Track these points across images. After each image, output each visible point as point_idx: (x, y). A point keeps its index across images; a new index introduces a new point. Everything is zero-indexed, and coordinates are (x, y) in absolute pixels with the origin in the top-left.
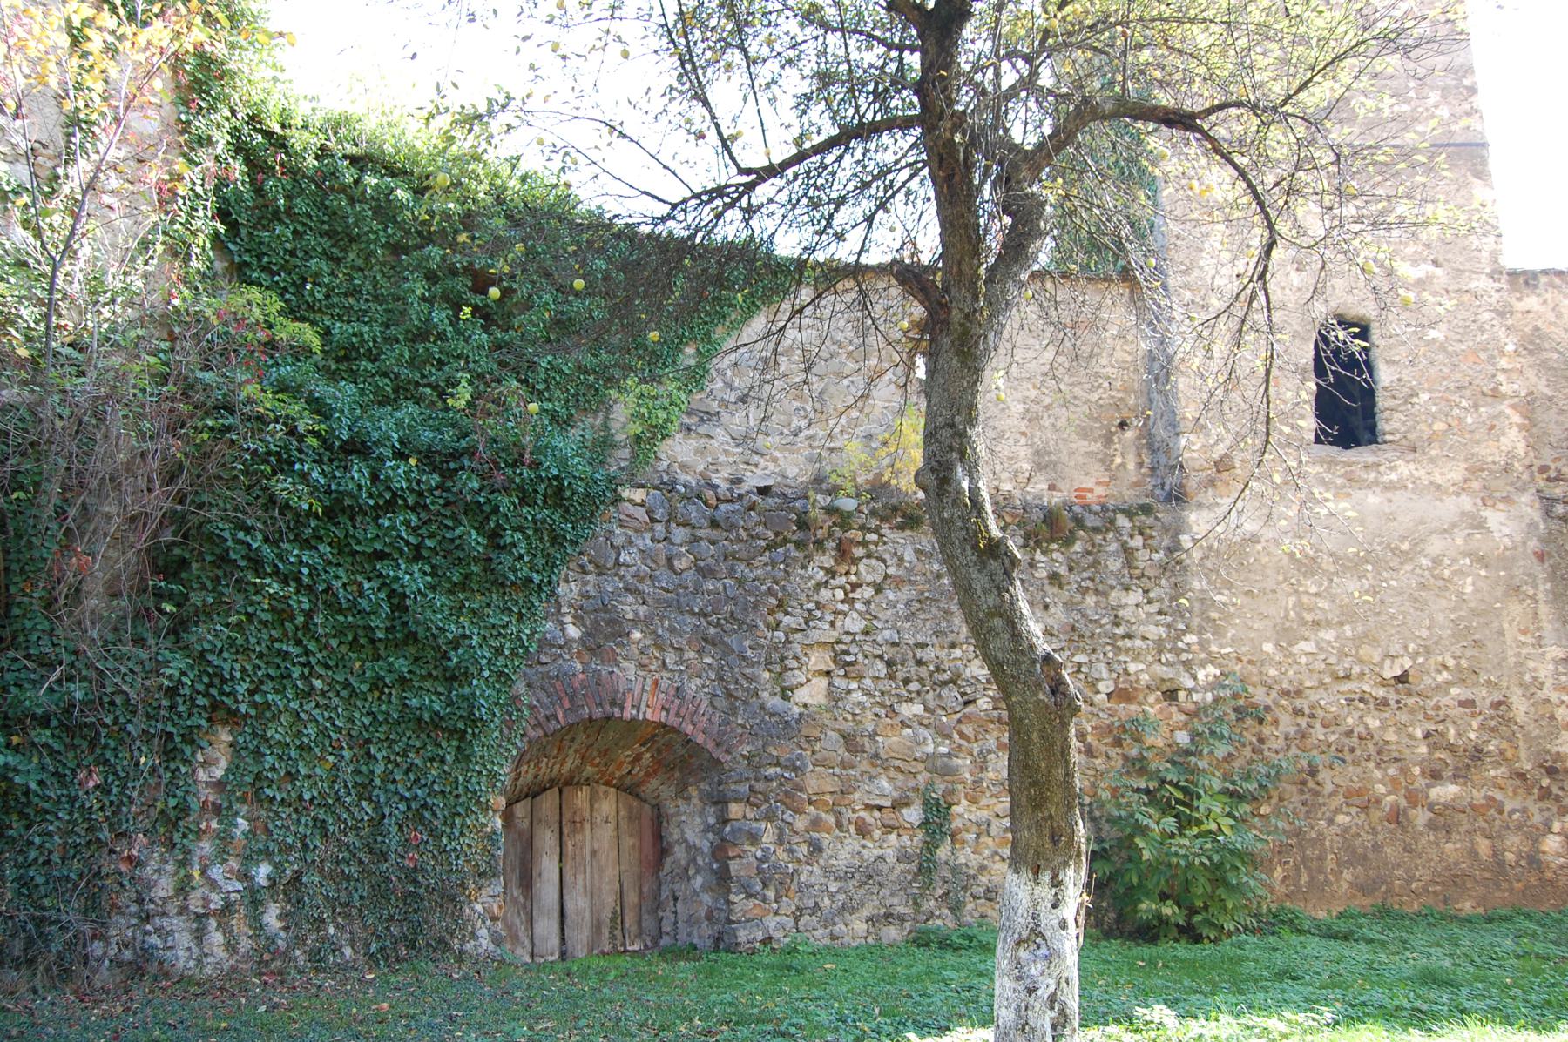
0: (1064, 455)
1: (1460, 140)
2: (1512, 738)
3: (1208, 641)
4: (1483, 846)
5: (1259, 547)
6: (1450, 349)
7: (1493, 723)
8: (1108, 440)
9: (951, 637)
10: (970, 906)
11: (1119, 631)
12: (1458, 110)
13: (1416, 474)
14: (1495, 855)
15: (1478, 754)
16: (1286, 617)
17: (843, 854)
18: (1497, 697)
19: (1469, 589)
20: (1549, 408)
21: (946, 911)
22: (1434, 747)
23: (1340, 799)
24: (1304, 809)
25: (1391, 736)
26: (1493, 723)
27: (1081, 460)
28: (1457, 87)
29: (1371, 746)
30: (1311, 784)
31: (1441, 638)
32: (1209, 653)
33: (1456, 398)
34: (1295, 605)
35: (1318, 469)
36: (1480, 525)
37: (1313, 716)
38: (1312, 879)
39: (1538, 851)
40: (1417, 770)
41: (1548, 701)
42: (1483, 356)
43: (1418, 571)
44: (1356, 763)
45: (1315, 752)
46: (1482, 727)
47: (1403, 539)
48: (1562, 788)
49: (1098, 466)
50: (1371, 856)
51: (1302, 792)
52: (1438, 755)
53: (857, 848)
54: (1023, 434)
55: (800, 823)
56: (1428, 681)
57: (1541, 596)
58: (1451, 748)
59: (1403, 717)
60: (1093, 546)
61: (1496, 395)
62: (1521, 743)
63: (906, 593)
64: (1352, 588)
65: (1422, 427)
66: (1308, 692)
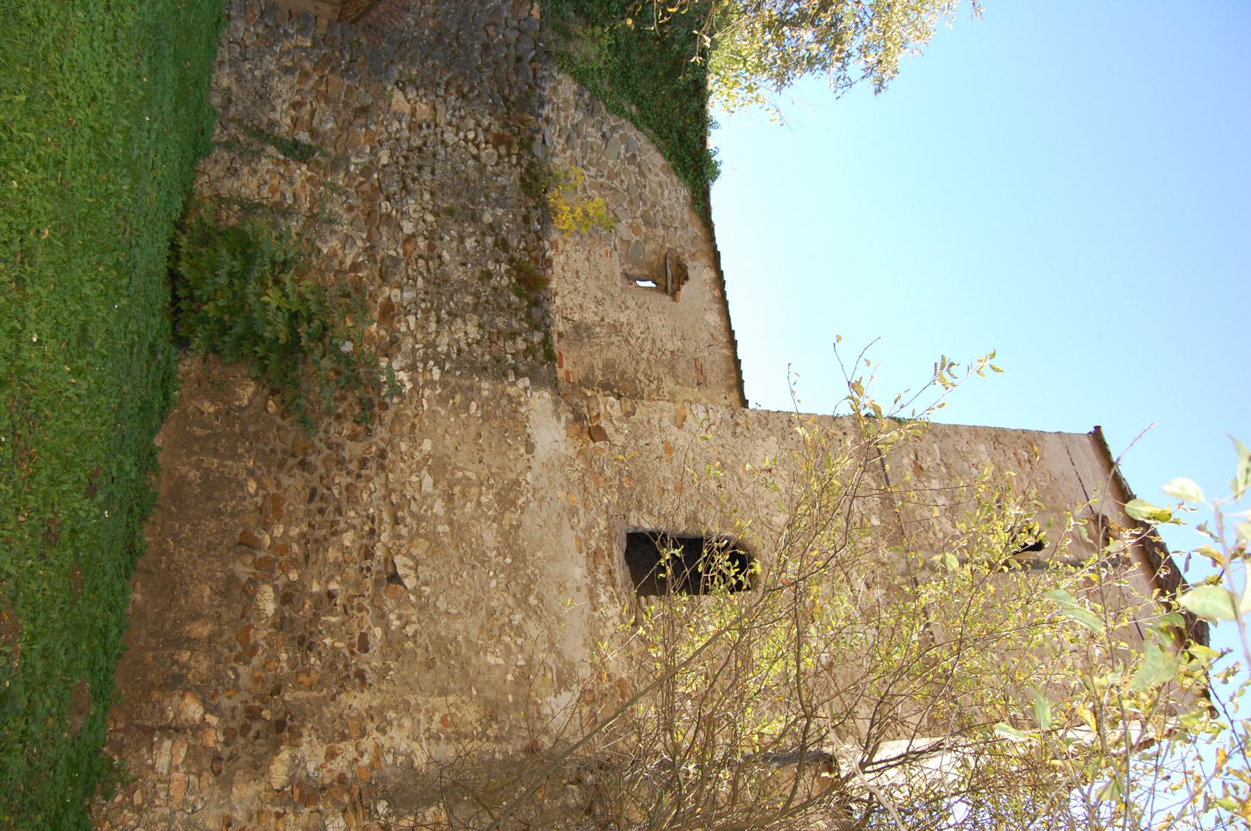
0: (587, 349)
3: (434, 389)
4: (202, 630)
5: (522, 450)
7: (341, 667)
9: (439, 194)
10: (226, 155)
13: (609, 624)
14: (188, 640)
15: (306, 644)
17: (281, 87)
18: (371, 677)
19: (491, 659)
21: (225, 139)
23: (272, 490)
24: (267, 449)
25: (332, 554)
27: (586, 360)
29: (324, 532)
30: (291, 462)
31: (436, 623)
32: (423, 388)
34: (468, 479)
35: (602, 523)
36: (562, 683)
37: (359, 476)
38: (197, 439)
39: (185, 690)
40: (294, 576)
41: (363, 733)
43: (507, 611)
44: (308, 513)
45: (322, 470)
47: (540, 598)
48: (257, 737)
50: (209, 506)
51: (284, 452)
53: (284, 97)
54: (603, 320)
55: (308, 66)
56: (390, 603)
59: (351, 571)
62: (314, 693)
63: (473, 174)
64: (490, 536)
66: (383, 476)
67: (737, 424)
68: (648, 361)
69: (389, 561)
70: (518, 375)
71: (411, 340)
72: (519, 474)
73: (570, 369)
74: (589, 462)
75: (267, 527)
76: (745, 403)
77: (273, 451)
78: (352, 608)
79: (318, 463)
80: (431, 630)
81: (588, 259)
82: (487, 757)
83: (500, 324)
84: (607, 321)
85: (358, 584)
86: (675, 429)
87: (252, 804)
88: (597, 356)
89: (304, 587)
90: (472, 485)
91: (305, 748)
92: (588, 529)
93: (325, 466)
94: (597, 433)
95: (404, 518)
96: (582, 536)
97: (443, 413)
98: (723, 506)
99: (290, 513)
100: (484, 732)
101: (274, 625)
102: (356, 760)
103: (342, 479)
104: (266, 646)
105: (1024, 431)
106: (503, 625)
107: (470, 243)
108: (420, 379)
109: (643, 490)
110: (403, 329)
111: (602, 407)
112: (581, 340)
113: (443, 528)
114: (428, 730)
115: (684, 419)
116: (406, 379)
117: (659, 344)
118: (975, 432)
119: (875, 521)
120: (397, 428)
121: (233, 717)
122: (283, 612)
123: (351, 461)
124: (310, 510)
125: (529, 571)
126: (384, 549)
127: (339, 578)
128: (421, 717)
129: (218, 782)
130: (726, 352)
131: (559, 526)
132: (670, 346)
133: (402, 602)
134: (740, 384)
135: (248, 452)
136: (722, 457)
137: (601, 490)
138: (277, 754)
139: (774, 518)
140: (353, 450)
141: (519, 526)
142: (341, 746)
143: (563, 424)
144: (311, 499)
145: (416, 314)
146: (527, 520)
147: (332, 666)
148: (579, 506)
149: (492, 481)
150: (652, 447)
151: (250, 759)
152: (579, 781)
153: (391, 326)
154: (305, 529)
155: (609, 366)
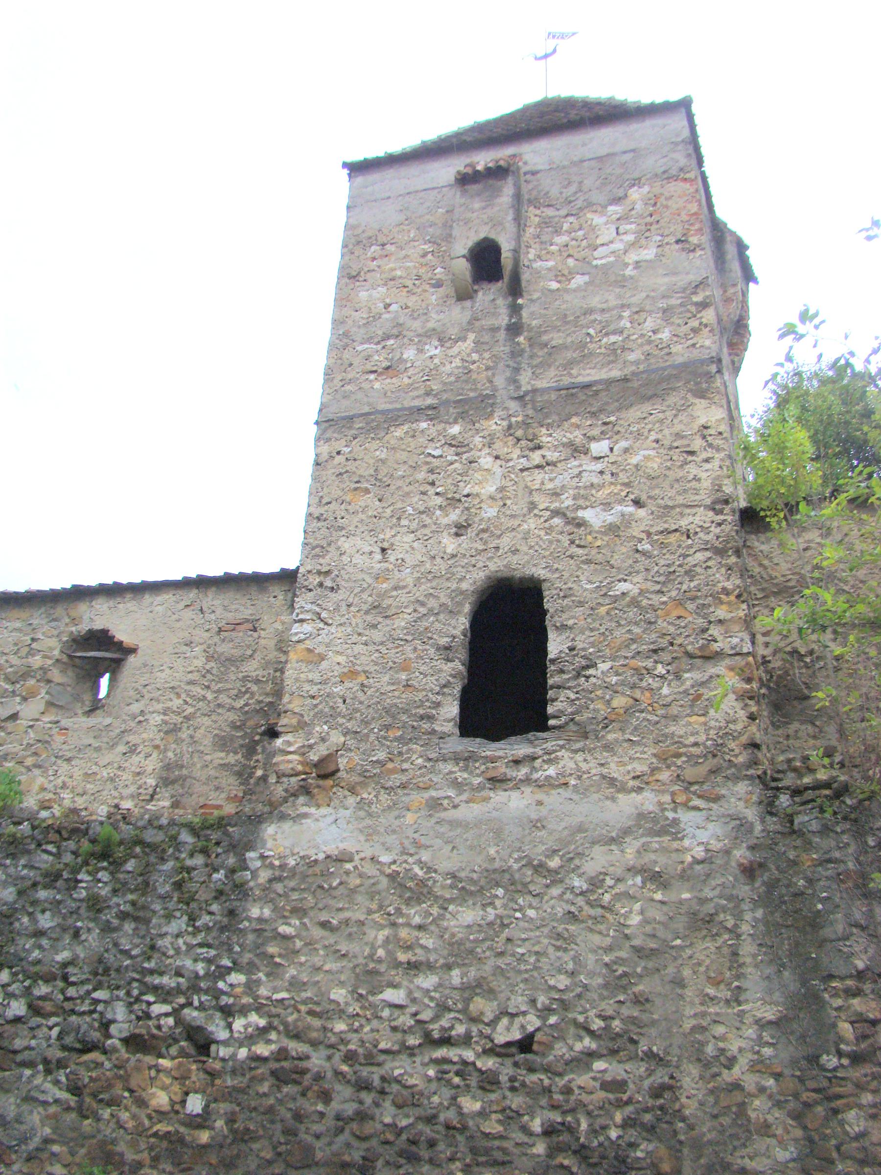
3: (258, 982)
5: (349, 866)
6: (645, 602)
7: (647, 1117)
13: (584, 766)
18: (661, 1076)
19: (635, 920)
26: (647, 1117)
32: (256, 998)
33: (649, 663)
34: (387, 941)
35: (449, 767)
36: (670, 829)
37: (382, 1092)
42: (691, 606)
49: (232, 780)
54: (157, 747)
56: (560, 1049)
57: (745, 928)
58: (582, 1152)
59: (516, 1101)
65: (599, 705)
67: (321, 585)
68: (219, 691)
71: (186, 1011)
73: (223, 796)
76: (288, 577)
80: (595, 996)
81: (69, 760)
82: (761, 927)
84: (158, 742)
86: (324, 665)
88: (208, 758)
90: (396, 935)
92: (456, 784)
94: (325, 771)
95: (443, 1029)
97: (292, 971)
100: (729, 931)
103: (387, 1114)
105: (345, 246)
107: (46, 921)
109: (405, 711)
112: (184, 778)
113: (456, 977)
114: (727, 1001)
117: (195, 676)
118: (343, 300)
119: (455, 429)
120: (314, 1035)
123: (361, 1102)
125: (516, 866)
127: (526, 1118)
131: (454, 824)
136: (365, 607)
141: (454, 876)
143: (313, 810)
145: (149, 1004)
146: (445, 865)
147: (651, 1130)
149: (391, 909)
150: (349, 695)
155: (222, 743)
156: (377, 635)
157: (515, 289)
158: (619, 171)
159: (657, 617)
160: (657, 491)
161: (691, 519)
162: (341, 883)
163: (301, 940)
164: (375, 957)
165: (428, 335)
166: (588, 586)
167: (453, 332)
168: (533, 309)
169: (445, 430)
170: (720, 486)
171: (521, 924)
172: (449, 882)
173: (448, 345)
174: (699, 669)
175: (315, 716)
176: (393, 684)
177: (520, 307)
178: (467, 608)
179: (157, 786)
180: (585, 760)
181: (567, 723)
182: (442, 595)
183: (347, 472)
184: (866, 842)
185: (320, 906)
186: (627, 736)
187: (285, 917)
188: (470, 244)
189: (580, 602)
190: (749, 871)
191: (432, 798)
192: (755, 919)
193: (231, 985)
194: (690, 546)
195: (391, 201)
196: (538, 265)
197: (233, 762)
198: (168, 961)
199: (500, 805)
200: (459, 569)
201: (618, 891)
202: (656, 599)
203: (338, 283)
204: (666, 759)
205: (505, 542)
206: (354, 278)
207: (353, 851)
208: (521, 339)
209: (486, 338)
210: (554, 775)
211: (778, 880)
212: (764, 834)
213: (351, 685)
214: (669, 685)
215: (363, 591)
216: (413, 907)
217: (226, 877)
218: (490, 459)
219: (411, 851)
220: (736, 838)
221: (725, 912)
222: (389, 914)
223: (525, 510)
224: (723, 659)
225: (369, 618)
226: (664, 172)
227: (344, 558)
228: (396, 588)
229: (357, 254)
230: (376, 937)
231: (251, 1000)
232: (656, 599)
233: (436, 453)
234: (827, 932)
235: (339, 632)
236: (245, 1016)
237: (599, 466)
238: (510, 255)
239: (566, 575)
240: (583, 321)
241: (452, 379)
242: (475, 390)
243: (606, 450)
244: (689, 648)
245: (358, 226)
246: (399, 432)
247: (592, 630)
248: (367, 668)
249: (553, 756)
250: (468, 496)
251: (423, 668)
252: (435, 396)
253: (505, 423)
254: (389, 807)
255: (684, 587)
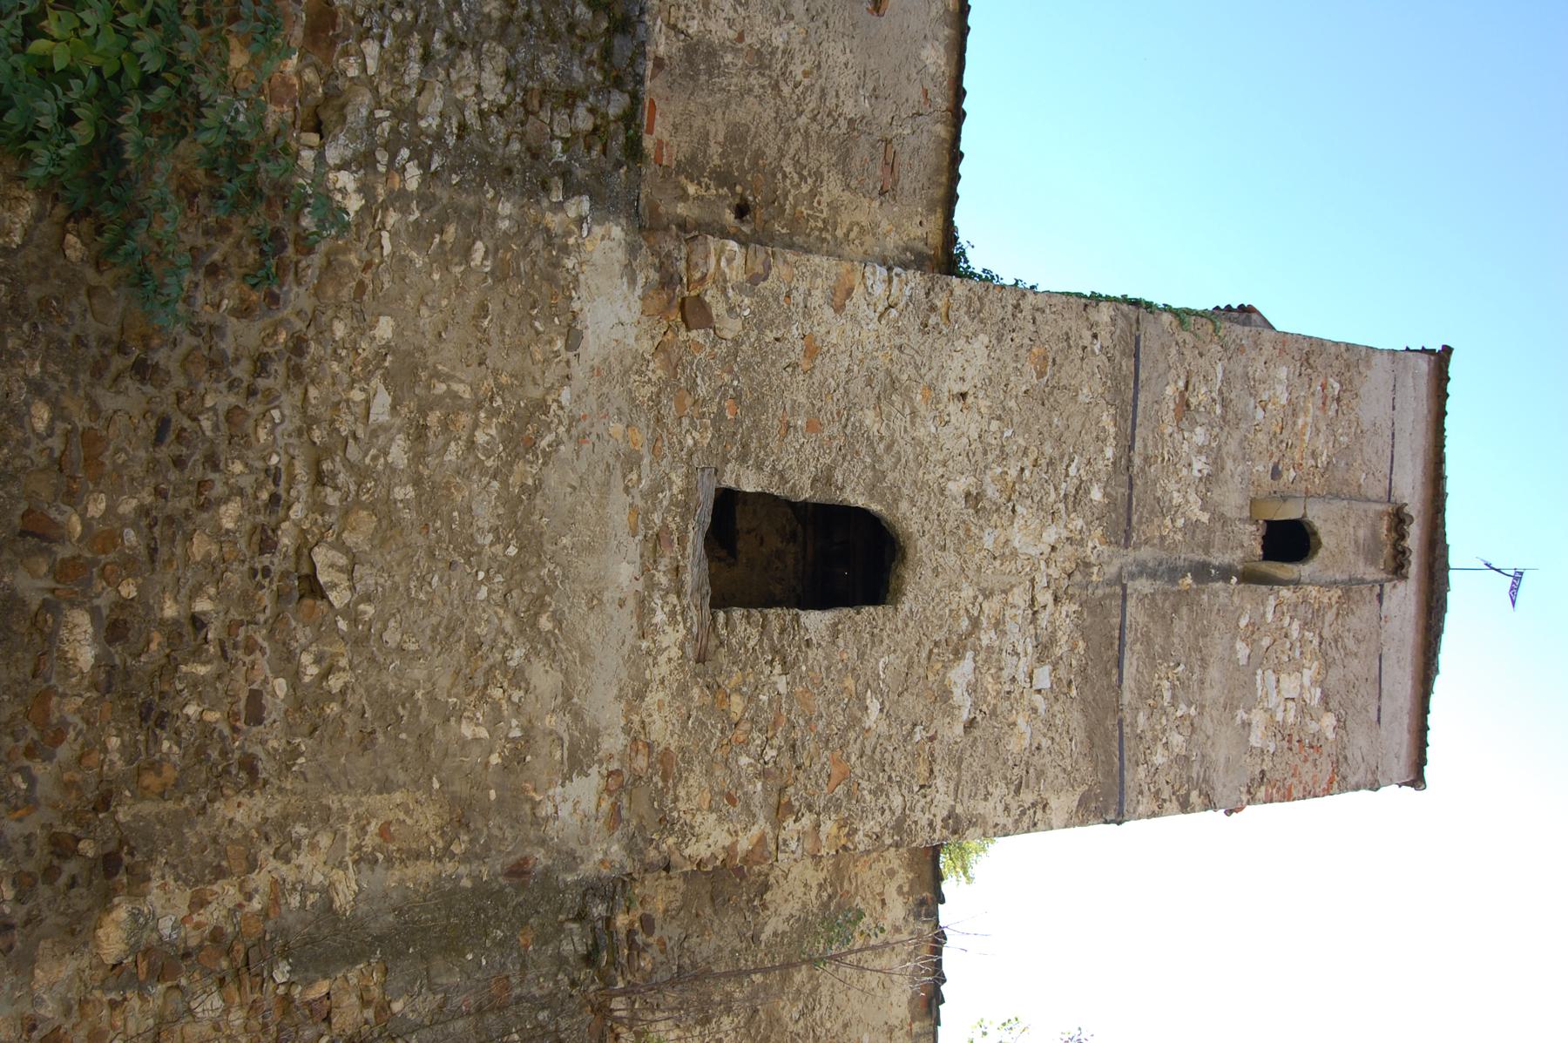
1: (1128, 776)
2: (181, 786)
3: (405, 211)
5: (559, 344)
6: (852, 735)
7: (215, 755)
8: (723, 178)
11: (438, 42)
12: (1161, 779)
13: (662, 659)
15: (154, 717)
16: (436, 375)
18: (266, 767)
19: (467, 730)
20: (741, 936)
22: (173, 633)
23: (82, 421)
24: (69, 337)
25: (201, 547)
27: (698, 122)
28: (1189, 778)
29: (184, 503)
30: (118, 362)
31: (382, 668)
34: (456, 396)
35: (678, 482)
36: (576, 763)
37: (251, 392)
40: (128, 590)
41: (253, 865)
42: (840, 791)
43: (502, 641)
44: (153, 466)
45: (179, 381)
46: (207, 730)
48: (73, 883)
51: (104, 341)
52: (157, 638)
54: (741, 38)
56: (303, 634)
57: (449, 867)
58: (170, 667)
60: (583, 39)
61: (781, 811)
62: (170, 805)
65: (736, 678)
67: (933, 308)
68: (807, 135)
69: (303, 551)
70: (571, 190)
72: (548, 390)
73: (666, 138)
74: (673, 367)
75: (72, 497)
77: (80, 341)
78: (235, 646)
79: (173, 367)
80: (371, 680)
82: (448, 886)
83: (549, 72)
84: (748, 40)
85: (246, 599)
86: (829, 312)
87: (69, 990)
88: (718, 116)
89: (149, 609)
91: (155, 896)
92: (656, 489)
93: (186, 372)
94: (694, 313)
95: (334, 475)
96: (640, 503)
98: (877, 459)
99: (119, 469)
100: (447, 848)
101: (94, 685)
102: (240, 906)
103: (218, 399)
104: (82, 725)
106: (492, 667)
108: (381, 190)
109: (756, 425)
110: (353, 72)
111: (712, 261)
112: (694, 78)
113: (403, 492)
114: (359, 848)
115: (849, 293)
116: (351, 186)
117: (831, 102)
119: (1096, 494)
120: (330, 291)
121: (29, 853)
122: (111, 656)
123: (237, 360)
124: (156, 461)
126: (295, 532)
128: (349, 828)
129: (9, 964)
130: (942, 130)
132: (849, 109)
133: (323, 630)
134: (951, 199)
135: (27, 345)
136: (895, 369)
137: (686, 421)
138: (109, 911)
139: (951, 485)
140: (241, 336)
142: (215, 888)
143: (639, 291)
144: (159, 439)
145: (382, 38)
146: (553, 478)
148: (644, 451)
149: (498, 402)
151: (61, 920)
152: (581, 917)
153: (328, 61)
154: (148, 500)
156: (857, 386)
157: (1250, 577)
158: (1359, 702)
159: (833, 750)
160: (981, 749)
161: (942, 789)
162: (538, 333)
163: (462, 273)
164: (434, 381)
165: (1217, 462)
166: (881, 664)
167: (1215, 495)
168: (1222, 594)
169: (1099, 480)
170: (975, 825)
171: (469, 580)
172: (530, 482)
173: (1202, 488)
174: (765, 800)
175: (764, 298)
176: (793, 407)
177: (1227, 579)
178: (875, 507)
179: (687, 35)
180: (670, 660)
181: (718, 636)
182: (896, 474)
183: (1070, 347)
184: (543, 1009)
185: (509, 302)
186: (694, 713)
187: (497, 250)
188: (1317, 524)
189: (864, 654)
190: (518, 871)
191: (641, 458)
192: (459, 877)
193: (404, 169)
194: (911, 791)
195: (1389, 410)
196: (1272, 601)
197: (710, 151)
198: (442, 73)
199: (623, 549)
200: (926, 498)
201: (505, 706)
202: (854, 749)
203: (1305, 337)
204: (661, 762)
205: (951, 559)
206: (1306, 360)
207: (580, 350)
208: (1189, 580)
209: (1199, 536)
210: (654, 621)
211: (505, 906)
212: (562, 886)
213: (798, 349)
214: (750, 765)
215: (917, 367)
216: (500, 432)
217: (558, 164)
218: (1052, 540)
219: (574, 432)
220: (559, 852)
221: (471, 841)
222: (492, 399)
223: (984, 585)
224: (774, 829)
225: (881, 375)
226: (1346, 758)
227: (962, 341)
228: (914, 413)
229: (1336, 363)
230: (462, 381)
231: (380, 199)
232: (854, 749)
233: (1072, 471)
234: (438, 962)
235: (868, 336)
236: (359, 190)
237: (1021, 677)
238: (1296, 576)
239: (898, 637)
240: (1196, 656)
241: (1159, 493)
242: (1140, 522)
243: (1037, 685)
244: (791, 790)
245: (1369, 367)
246: (1106, 420)
247: (828, 668)
248: (817, 372)
249: (679, 618)
250: (1014, 511)
251: (808, 448)
252: (1142, 470)
253: (1093, 559)
254: (633, 399)
255: (864, 784)
